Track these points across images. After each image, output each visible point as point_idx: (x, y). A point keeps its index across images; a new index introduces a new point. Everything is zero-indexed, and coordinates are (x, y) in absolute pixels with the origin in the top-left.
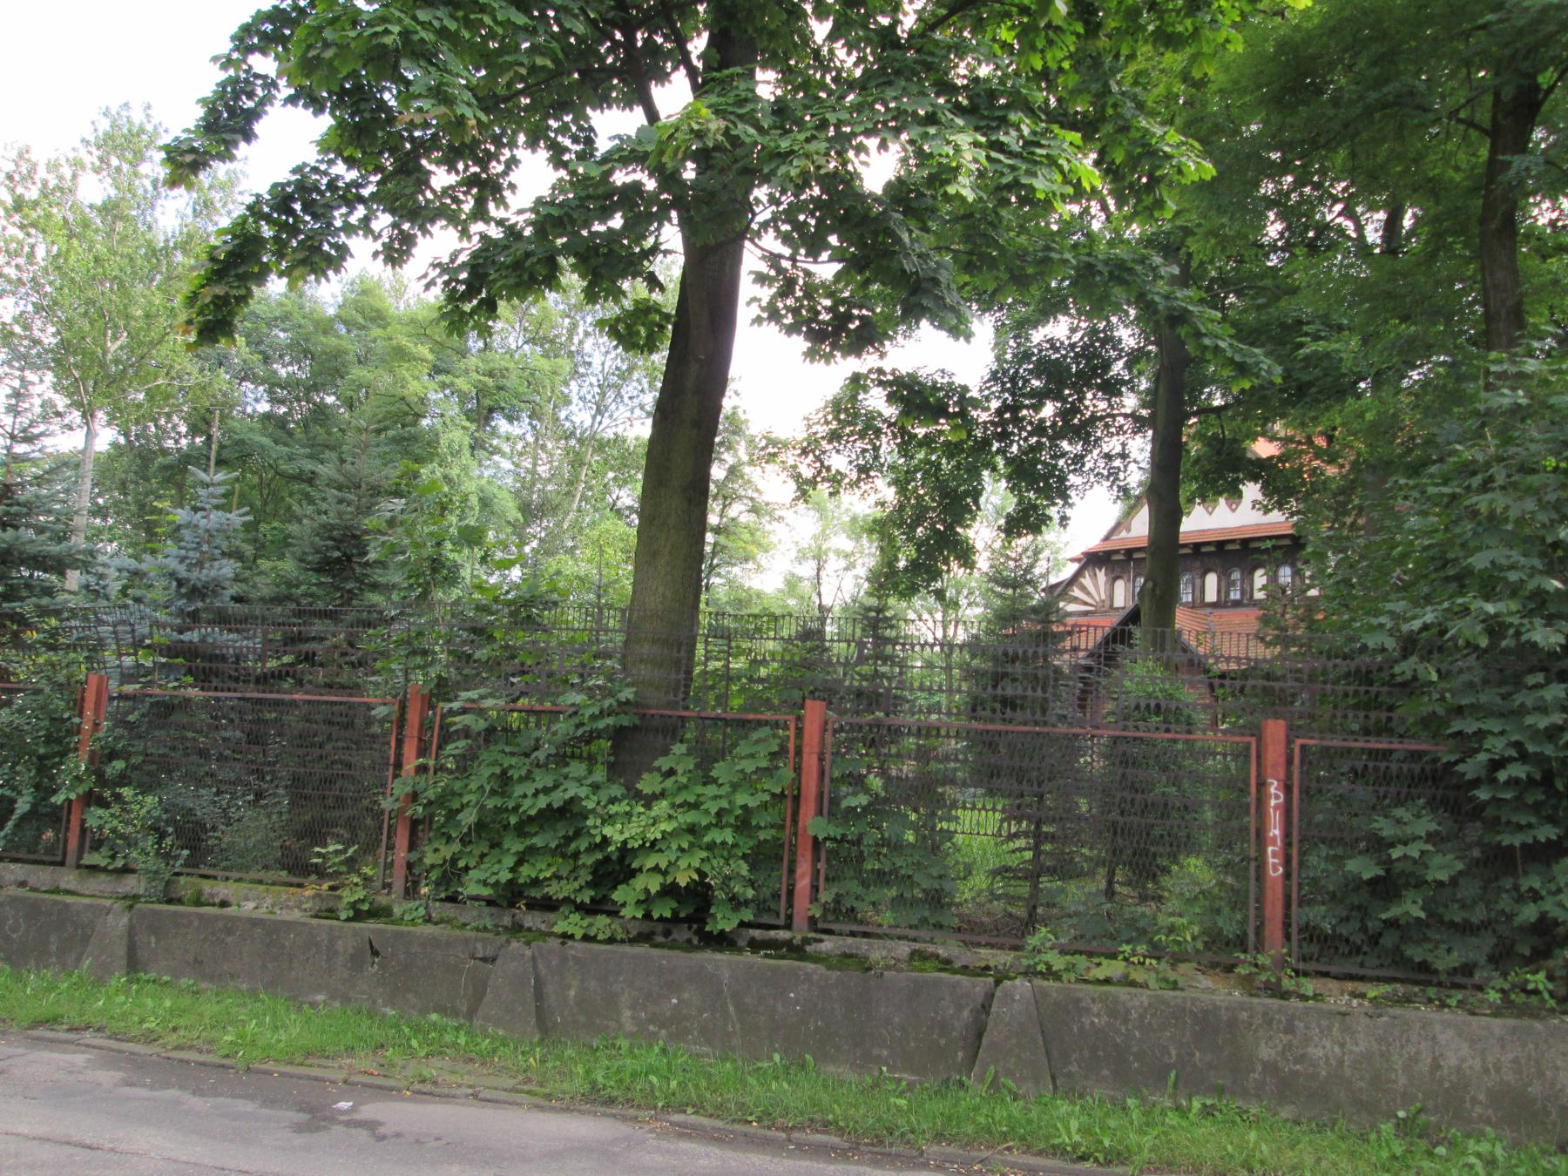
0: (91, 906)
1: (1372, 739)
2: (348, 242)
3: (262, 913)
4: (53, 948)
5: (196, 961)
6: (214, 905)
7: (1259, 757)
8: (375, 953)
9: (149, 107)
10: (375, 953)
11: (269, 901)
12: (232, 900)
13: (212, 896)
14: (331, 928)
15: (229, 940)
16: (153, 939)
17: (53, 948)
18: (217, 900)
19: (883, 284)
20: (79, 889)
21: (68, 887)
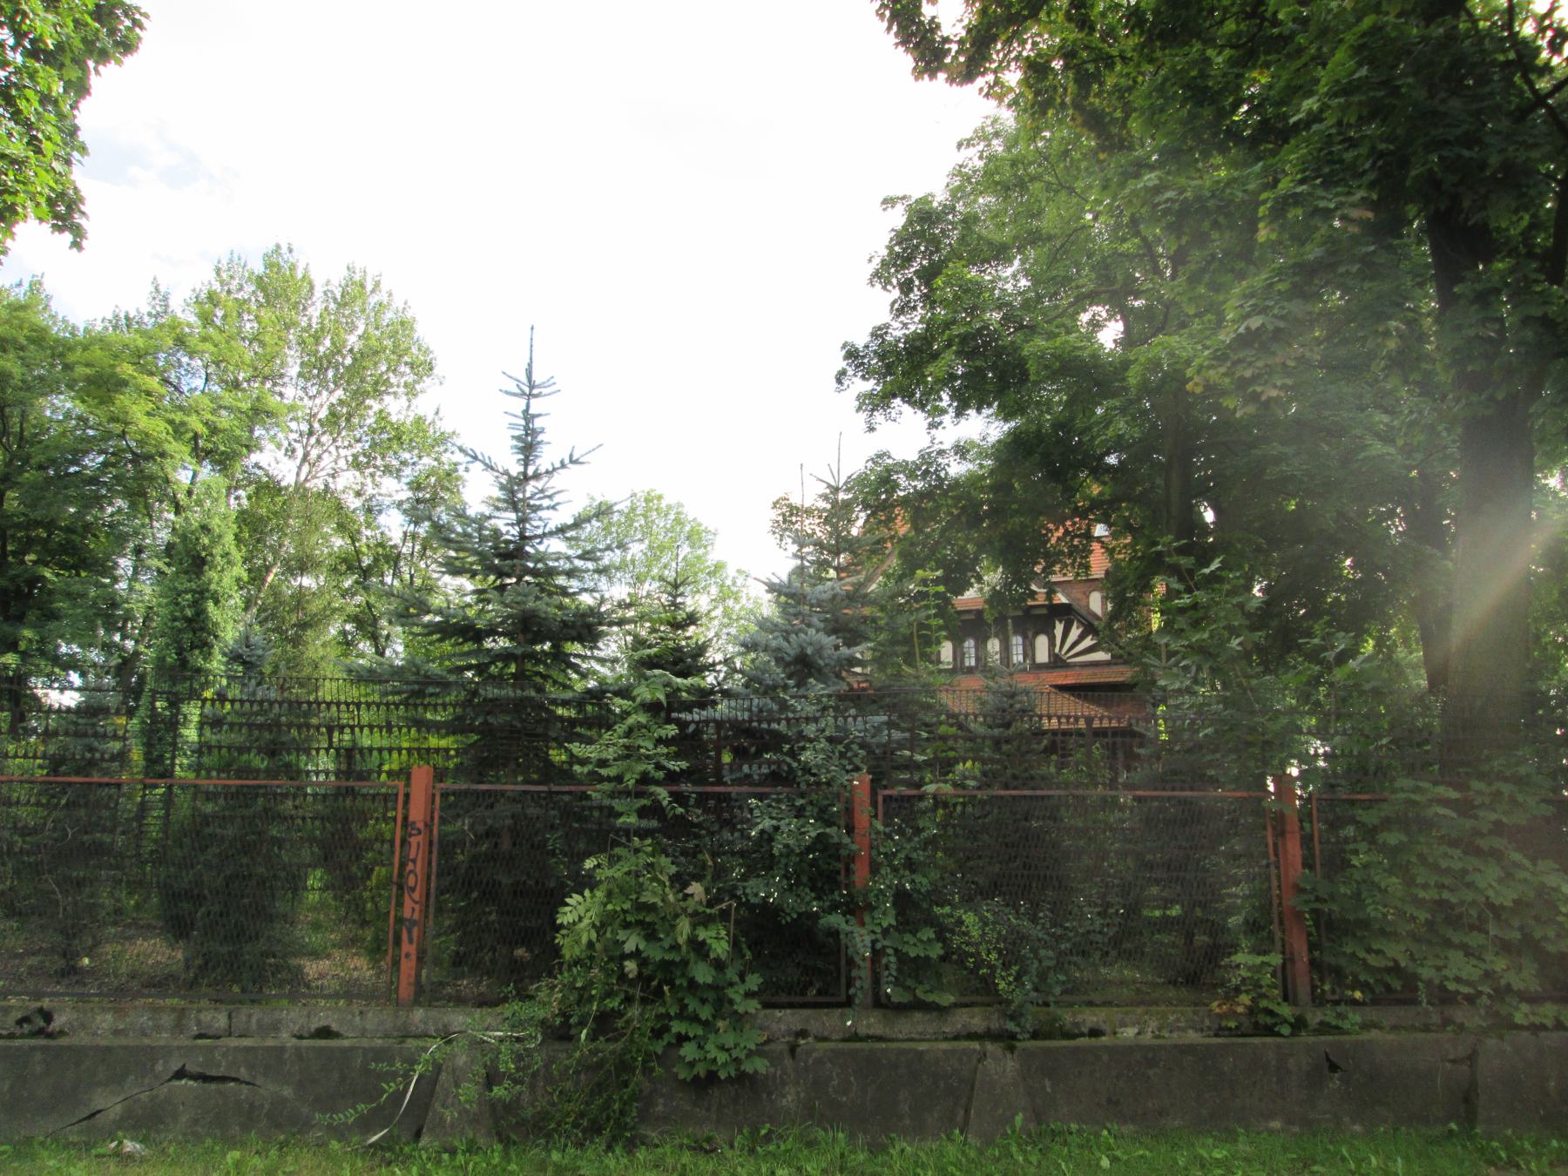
0: (953, 1052)
1: (1288, 828)
2: (423, 406)
3: (1147, 1038)
4: (905, 1108)
5: (1109, 1101)
6: (1082, 1035)
7: (428, 895)
8: (1334, 1068)
9: (76, 245)
10: (1334, 1068)
11: (1153, 1024)
12: (1106, 1028)
13: (1076, 1025)
14: (1278, 1046)
15: (1151, 1072)
16: (1047, 1083)
17: (905, 1108)
18: (1085, 1030)
19: (1101, 404)
20: (888, 1032)
21: (871, 1032)
